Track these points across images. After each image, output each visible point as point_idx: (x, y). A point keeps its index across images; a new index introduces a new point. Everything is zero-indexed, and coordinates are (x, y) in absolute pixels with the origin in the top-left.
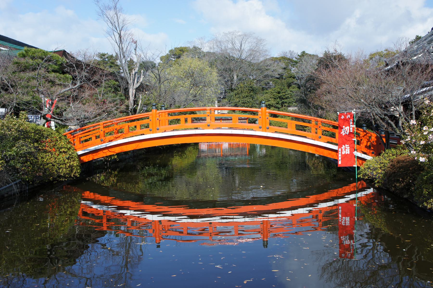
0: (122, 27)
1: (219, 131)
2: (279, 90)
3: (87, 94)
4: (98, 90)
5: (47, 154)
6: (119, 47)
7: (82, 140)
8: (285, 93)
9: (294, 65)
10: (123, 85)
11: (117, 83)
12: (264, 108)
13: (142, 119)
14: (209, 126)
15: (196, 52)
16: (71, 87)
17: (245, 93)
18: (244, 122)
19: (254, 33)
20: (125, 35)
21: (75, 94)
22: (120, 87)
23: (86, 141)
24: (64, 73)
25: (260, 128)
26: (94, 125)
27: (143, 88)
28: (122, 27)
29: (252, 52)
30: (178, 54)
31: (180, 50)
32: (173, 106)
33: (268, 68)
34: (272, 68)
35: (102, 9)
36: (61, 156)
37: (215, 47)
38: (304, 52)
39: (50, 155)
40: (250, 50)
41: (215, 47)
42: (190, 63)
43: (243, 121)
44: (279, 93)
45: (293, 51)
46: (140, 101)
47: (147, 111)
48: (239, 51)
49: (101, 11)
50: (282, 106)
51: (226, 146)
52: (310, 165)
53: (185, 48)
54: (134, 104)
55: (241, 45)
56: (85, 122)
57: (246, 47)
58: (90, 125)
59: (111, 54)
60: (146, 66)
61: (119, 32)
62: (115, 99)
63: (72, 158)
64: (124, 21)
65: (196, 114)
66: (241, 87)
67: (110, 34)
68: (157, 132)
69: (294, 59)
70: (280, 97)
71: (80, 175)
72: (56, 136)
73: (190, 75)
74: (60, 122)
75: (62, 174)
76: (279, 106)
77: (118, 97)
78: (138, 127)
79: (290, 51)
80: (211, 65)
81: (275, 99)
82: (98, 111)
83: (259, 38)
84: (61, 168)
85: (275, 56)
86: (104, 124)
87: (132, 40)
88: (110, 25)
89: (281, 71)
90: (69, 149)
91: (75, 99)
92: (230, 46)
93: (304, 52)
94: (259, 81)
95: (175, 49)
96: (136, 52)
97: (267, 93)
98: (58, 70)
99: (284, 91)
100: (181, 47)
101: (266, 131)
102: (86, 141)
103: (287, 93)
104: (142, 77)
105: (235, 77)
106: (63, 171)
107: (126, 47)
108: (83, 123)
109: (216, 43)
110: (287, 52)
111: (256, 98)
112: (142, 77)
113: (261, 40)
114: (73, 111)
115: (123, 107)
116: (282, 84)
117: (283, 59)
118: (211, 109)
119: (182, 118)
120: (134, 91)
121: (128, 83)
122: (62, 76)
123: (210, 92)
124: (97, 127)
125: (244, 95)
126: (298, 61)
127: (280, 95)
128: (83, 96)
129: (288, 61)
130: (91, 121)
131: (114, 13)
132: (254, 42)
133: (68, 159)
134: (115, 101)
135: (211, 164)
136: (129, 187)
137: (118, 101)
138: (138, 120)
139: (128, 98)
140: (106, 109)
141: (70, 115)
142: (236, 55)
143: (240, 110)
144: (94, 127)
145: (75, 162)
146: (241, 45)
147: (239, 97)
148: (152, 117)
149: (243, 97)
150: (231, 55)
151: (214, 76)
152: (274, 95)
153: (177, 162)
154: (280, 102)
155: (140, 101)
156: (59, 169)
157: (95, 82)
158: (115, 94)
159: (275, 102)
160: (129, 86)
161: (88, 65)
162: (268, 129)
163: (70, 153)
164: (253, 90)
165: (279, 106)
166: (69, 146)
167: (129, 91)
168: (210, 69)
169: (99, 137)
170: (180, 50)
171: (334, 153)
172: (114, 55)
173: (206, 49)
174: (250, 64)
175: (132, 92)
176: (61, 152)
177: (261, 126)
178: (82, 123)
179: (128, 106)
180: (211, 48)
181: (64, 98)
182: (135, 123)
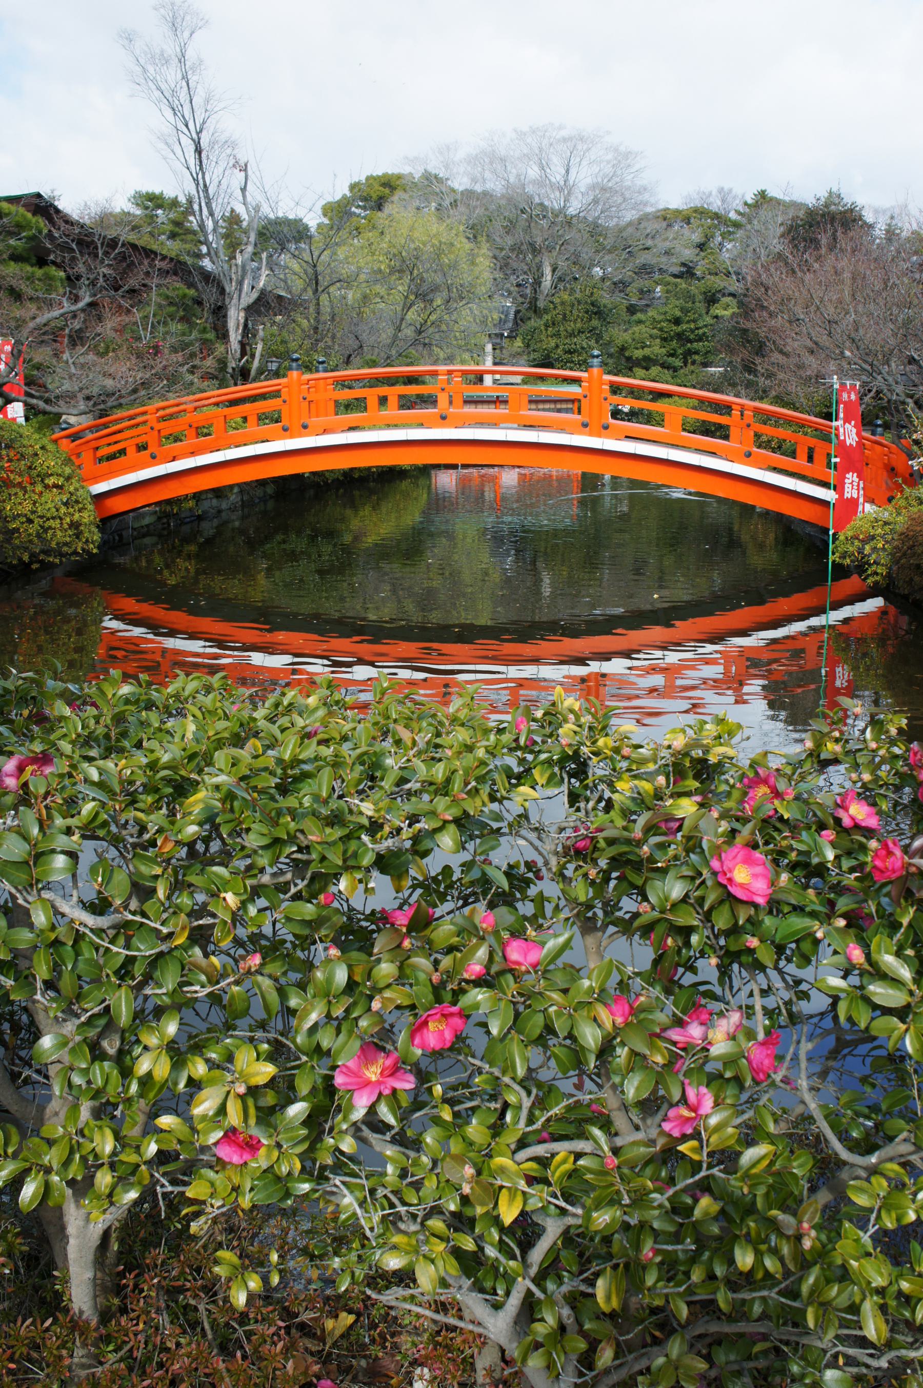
0: (204, 123)
1: (511, 432)
2: (678, 313)
3: (108, 326)
4: (137, 315)
5: (13, 491)
6: (196, 181)
7: (100, 453)
8: (694, 321)
9: (730, 233)
10: (210, 296)
11: (192, 292)
12: (596, 371)
13: (263, 396)
14: (443, 418)
15: (430, 185)
16: (67, 306)
17: (575, 321)
18: (567, 411)
19: (608, 133)
20: (212, 144)
21: (77, 325)
22: (200, 298)
23: (111, 457)
24: (42, 262)
25: (585, 425)
26: (131, 412)
27: (267, 305)
28: (204, 123)
29: (603, 192)
30: (377, 194)
31: (384, 185)
32: (355, 360)
33: (649, 243)
34: (662, 245)
35: (142, 61)
36: (47, 496)
37: (487, 175)
38: (762, 194)
39: (21, 494)
40: (593, 187)
41: (487, 175)
42: (406, 223)
43: (564, 406)
44: (677, 321)
45: (730, 191)
46: (260, 347)
47: (277, 374)
48: (561, 190)
49: (139, 69)
50: (685, 364)
51: (509, 479)
52: (745, 538)
53: (399, 177)
54: (243, 353)
55: (567, 171)
56: (109, 404)
57: (584, 177)
58: (120, 413)
59: (173, 195)
60: (280, 235)
61: (195, 136)
62: (187, 339)
63: (77, 502)
64: (207, 101)
65: (423, 383)
66: (563, 303)
67: (170, 141)
68: (312, 432)
69: (733, 216)
70: (679, 336)
71: (98, 548)
72: (32, 442)
73: (403, 265)
74: (41, 404)
75: (54, 545)
76: (678, 363)
77: (195, 334)
78: (252, 419)
79: (721, 190)
80: (475, 232)
81: (664, 339)
82: (140, 375)
83: (622, 149)
84: (50, 528)
85: (673, 205)
86: (158, 410)
87: (232, 162)
88: (169, 113)
89: (688, 254)
90: (68, 479)
91: (77, 339)
92: (533, 172)
93: (762, 194)
94: (621, 286)
95: (368, 178)
96: (244, 196)
97: (640, 322)
98: (25, 254)
99: (691, 316)
100: (385, 175)
101: (599, 436)
102: (111, 457)
103: (700, 323)
104: (265, 272)
105: (547, 271)
106: (60, 535)
107: (215, 183)
108: (102, 406)
109: (491, 163)
110: (710, 194)
111: (606, 337)
112: (265, 272)
113: (627, 155)
114: (71, 372)
115: (210, 363)
116: (691, 298)
117: (696, 215)
118: (450, 372)
119: (372, 395)
120: (242, 314)
121: (222, 291)
122: (39, 272)
123: (467, 316)
124: (140, 419)
125: (570, 326)
126: (744, 221)
127: (679, 329)
128: (99, 330)
129: (707, 221)
130: (122, 401)
131: (179, 76)
132: (608, 162)
133: (66, 504)
134: (187, 345)
135: (467, 527)
136: (233, 588)
137: (196, 347)
138: (253, 399)
139: (224, 336)
140: (165, 367)
141: (67, 386)
142: (554, 201)
143: (556, 377)
144: (131, 418)
145: (85, 514)
146: (567, 171)
147: (557, 335)
148: (289, 393)
149: (572, 335)
150: (537, 200)
151: (483, 269)
152: (661, 330)
153: (376, 525)
154: (680, 351)
155: (260, 347)
156: (46, 531)
157: (132, 291)
158: (186, 326)
159: (664, 351)
160: (227, 301)
161: (113, 243)
162: (606, 428)
163: (72, 489)
164: (597, 312)
165: (678, 363)
166: (68, 470)
167: (225, 316)
168: (468, 246)
169: (145, 447)
170: (384, 185)
171: (818, 508)
172: (182, 199)
173: (460, 183)
174: (595, 231)
175: (235, 318)
176: (47, 487)
177: (586, 420)
178: (102, 406)
179: (223, 363)
180: (474, 180)
181: (51, 335)
182: (247, 408)
